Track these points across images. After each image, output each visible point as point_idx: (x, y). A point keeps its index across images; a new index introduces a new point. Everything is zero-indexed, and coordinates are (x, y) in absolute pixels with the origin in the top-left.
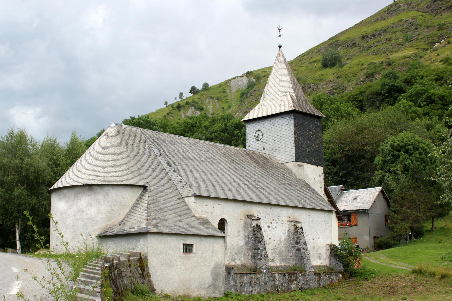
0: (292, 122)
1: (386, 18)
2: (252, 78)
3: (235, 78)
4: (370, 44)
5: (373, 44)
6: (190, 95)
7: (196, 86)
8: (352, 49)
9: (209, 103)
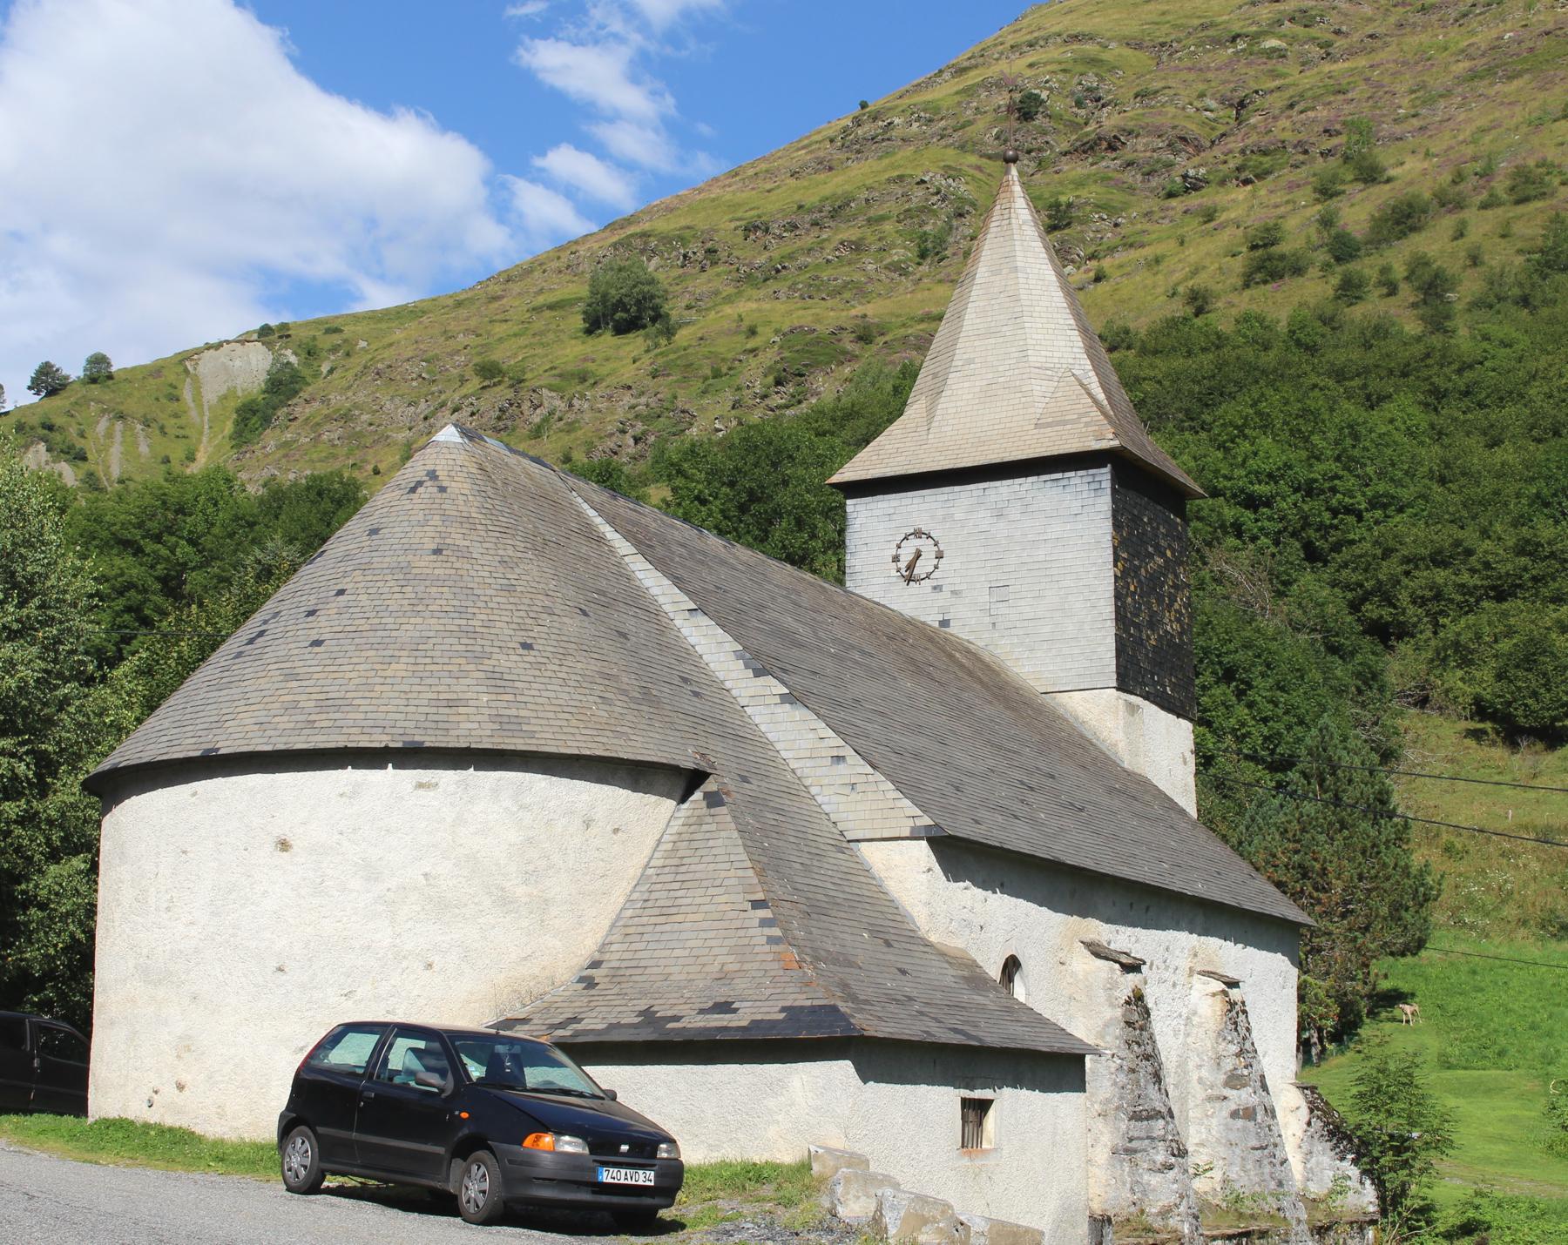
0: (1105, 503)
1: (834, 163)
2: (289, 352)
3: (219, 345)
4: (776, 255)
5: (791, 257)
6: (31, 398)
7: (57, 363)
8: (703, 270)
9: (109, 435)
